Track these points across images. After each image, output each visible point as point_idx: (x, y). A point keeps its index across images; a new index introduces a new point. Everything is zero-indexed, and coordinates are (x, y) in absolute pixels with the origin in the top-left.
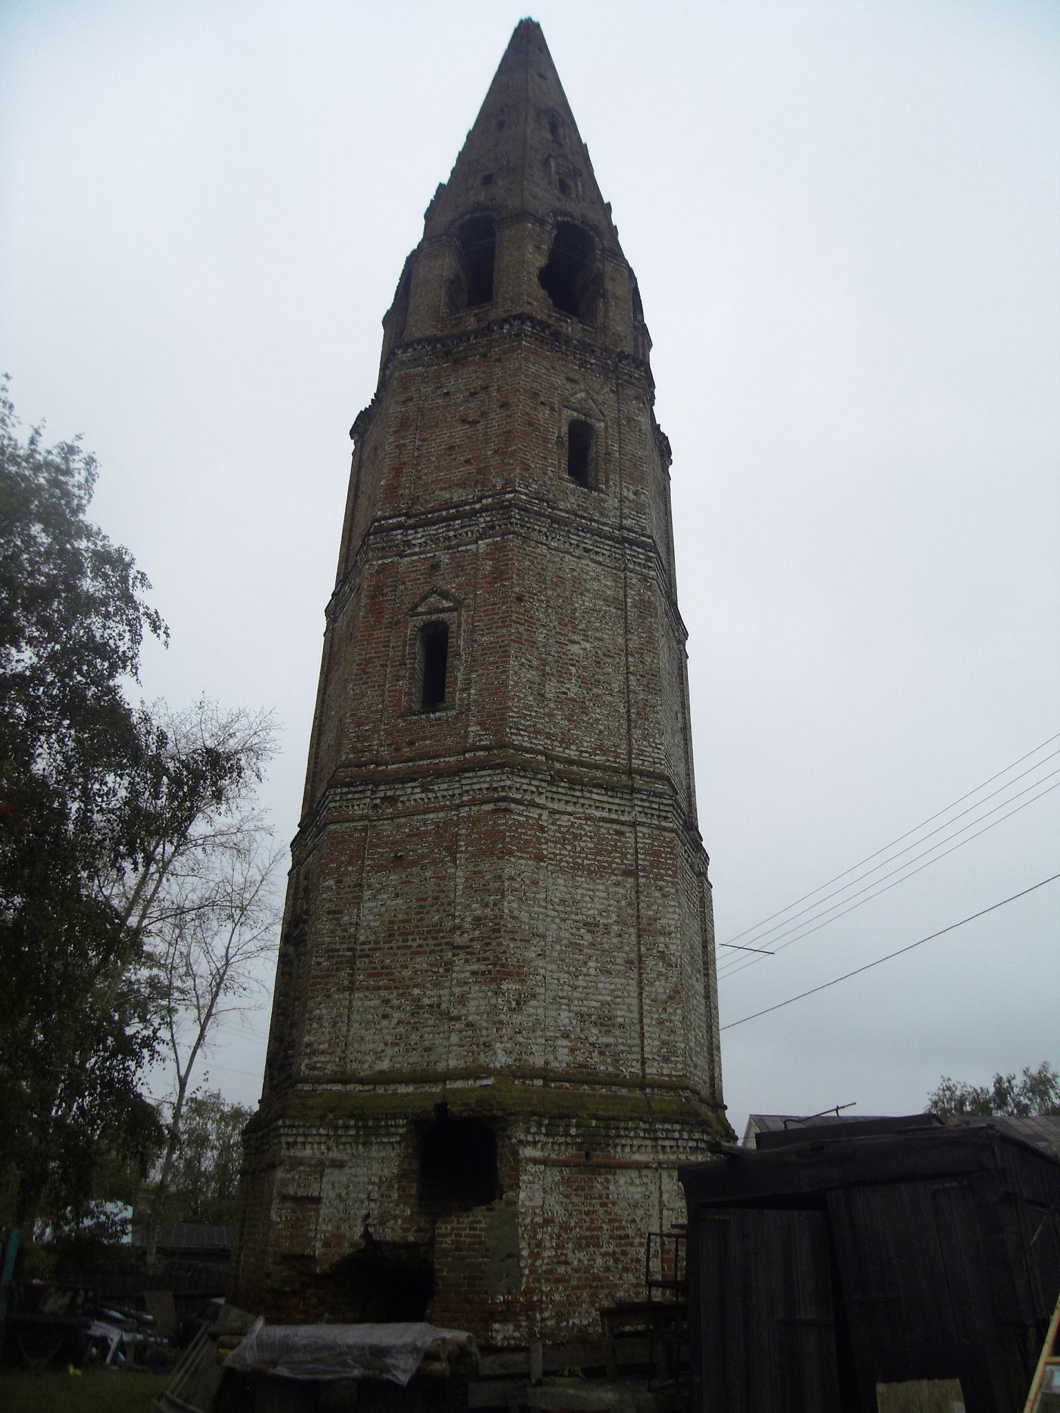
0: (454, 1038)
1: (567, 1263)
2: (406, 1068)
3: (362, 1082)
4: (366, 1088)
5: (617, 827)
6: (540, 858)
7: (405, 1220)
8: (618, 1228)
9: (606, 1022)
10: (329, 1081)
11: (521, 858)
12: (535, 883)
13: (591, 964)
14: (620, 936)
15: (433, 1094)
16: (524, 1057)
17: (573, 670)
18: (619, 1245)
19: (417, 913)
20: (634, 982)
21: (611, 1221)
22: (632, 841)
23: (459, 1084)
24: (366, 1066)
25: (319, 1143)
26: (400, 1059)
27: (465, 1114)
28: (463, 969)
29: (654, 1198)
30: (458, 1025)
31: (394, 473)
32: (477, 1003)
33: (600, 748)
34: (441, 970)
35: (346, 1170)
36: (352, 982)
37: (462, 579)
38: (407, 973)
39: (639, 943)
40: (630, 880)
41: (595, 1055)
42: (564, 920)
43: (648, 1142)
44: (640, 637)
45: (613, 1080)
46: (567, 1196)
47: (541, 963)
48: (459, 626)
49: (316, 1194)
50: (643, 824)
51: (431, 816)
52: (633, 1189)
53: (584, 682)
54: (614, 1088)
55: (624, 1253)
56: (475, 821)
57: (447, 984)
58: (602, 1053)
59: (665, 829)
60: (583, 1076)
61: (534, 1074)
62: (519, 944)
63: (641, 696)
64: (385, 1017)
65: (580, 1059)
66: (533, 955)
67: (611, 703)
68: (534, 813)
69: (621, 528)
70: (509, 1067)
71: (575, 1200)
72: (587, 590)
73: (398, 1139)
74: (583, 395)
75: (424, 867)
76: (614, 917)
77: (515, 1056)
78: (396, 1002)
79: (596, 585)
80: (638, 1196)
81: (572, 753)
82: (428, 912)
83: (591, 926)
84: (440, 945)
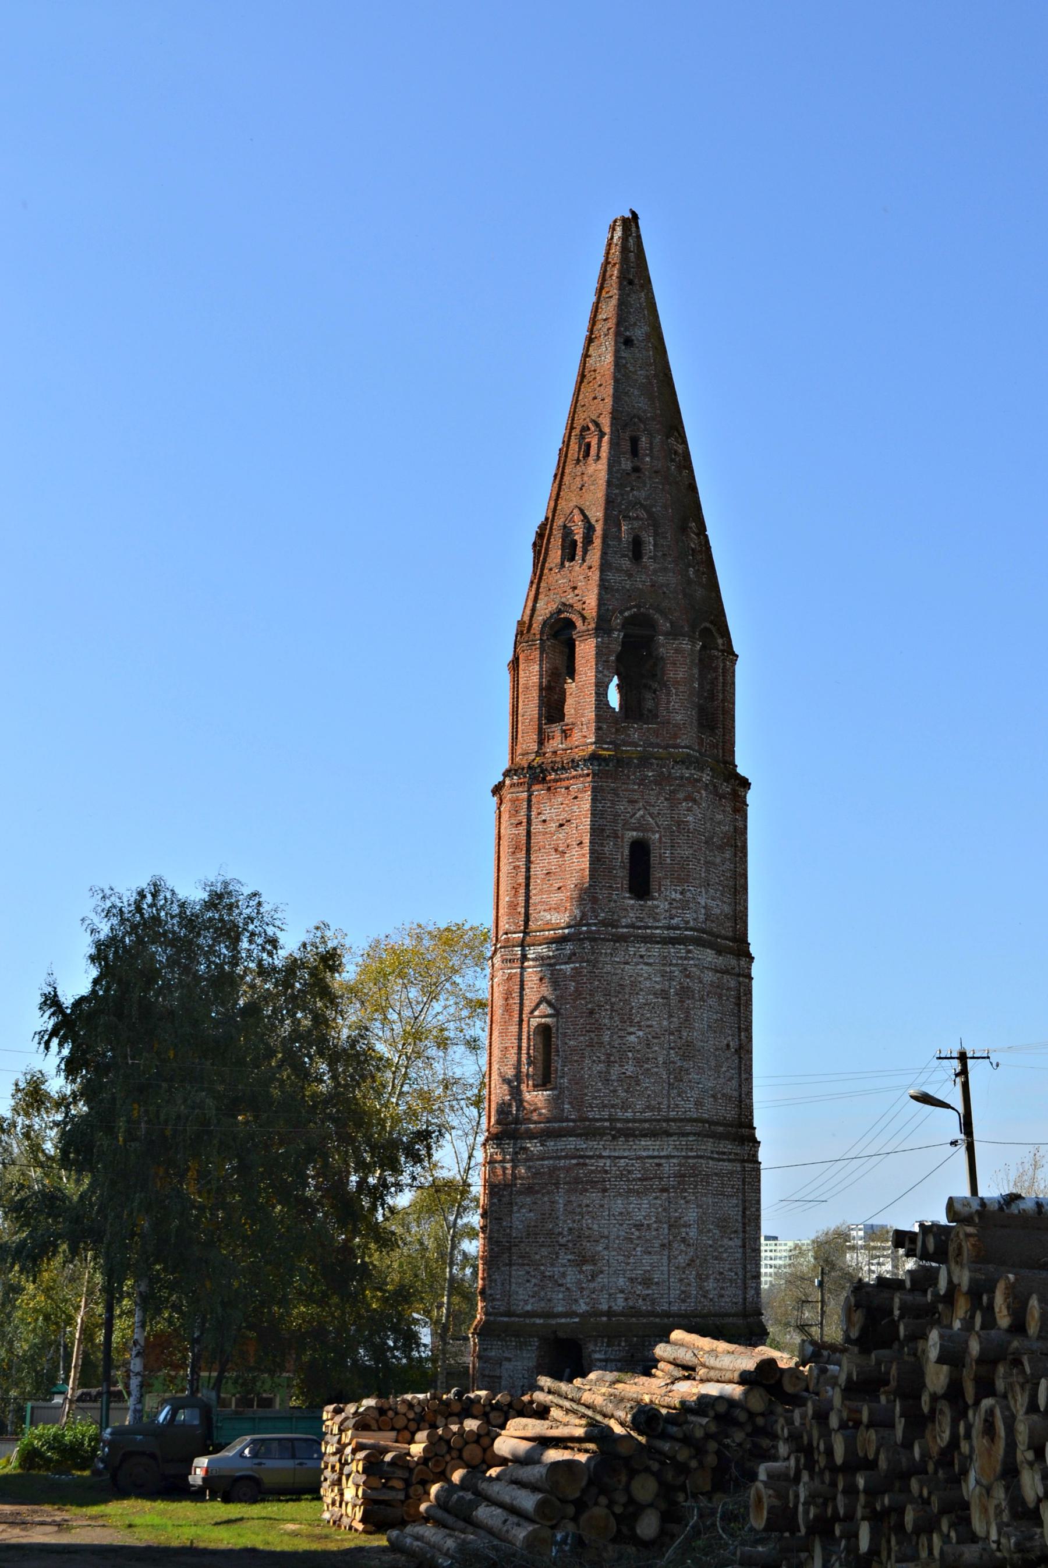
0: (561, 1296)
2: (540, 1310)
3: (518, 1316)
5: (657, 1161)
9: (647, 1282)
10: (502, 1316)
12: (602, 1206)
17: (630, 1054)
28: (564, 1258)
30: (562, 1289)
32: (571, 1277)
33: (649, 1108)
36: (510, 1261)
38: (538, 1257)
40: (665, 1194)
42: (621, 1225)
44: (679, 1018)
47: (606, 1253)
48: (557, 1030)
51: (546, 1162)
53: (639, 1062)
56: (568, 1169)
58: (644, 1300)
59: (689, 1157)
60: (633, 1312)
61: (602, 1314)
63: (679, 1064)
64: (528, 1281)
65: (631, 1304)
67: (657, 1073)
72: (641, 990)
74: (641, 812)
75: (543, 1195)
76: (654, 1219)
79: (648, 984)
81: (629, 1115)
83: (639, 1226)
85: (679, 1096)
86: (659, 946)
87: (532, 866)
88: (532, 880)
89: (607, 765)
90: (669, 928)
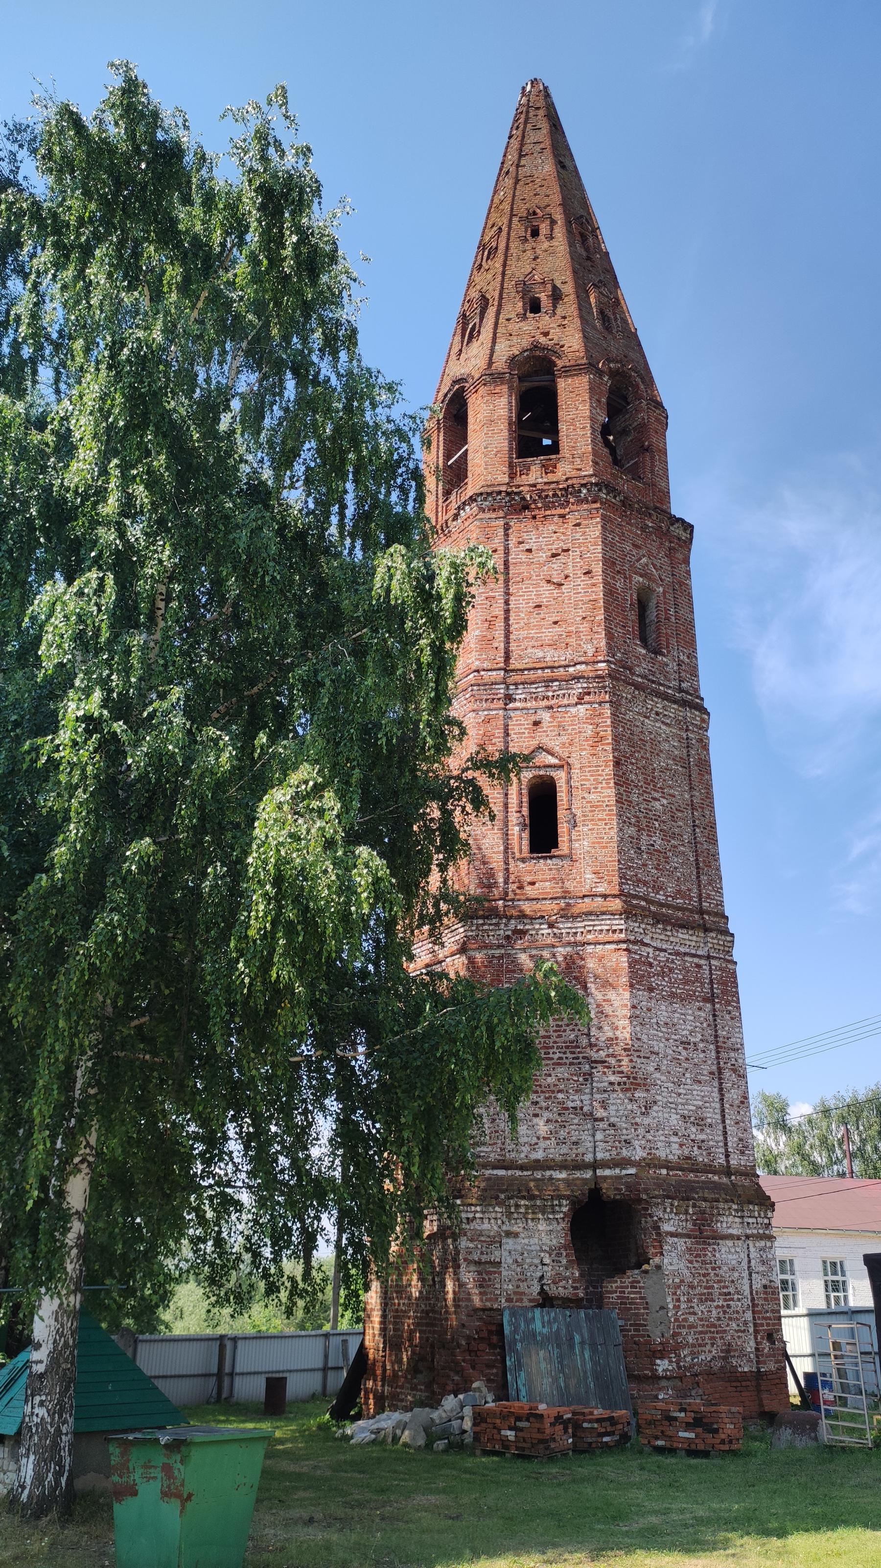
1: (695, 1314)
3: (522, 1168)
4: (525, 1173)
5: (696, 960)
6: (651, 990)
7: (574, 1281)
8: (724, 1287)
9: (700, 1123)
10: (495, 1167)
11: (639, 990)
12: (649, 1010)
13: (688, 1075)
14: (704, 1052)
15: (585, 1180)
16: (653, 1151)
18: (725, 1300)
19: (555, 1031)
20: (716, 1090)
21: (719, 1282)
22: (707, 972)
23: (607, 1172)
24: (523, 1155)
25: (496, 1219)
26: (552, 1150)
27: (618, 1197)
29: (745, 1264)
30: (601, 1125)
31: (486, 625)
34: (581, 1079)
35: (520, 1240)
37: (564, 739)
39: (718, 1058)
40: (708, 1005)
41: (695, 1148)
42: (668, 1040)
43: (737, 1220)
45: (708, 1169)
46: (691, 1262)
49: (498, 1260)
50: (714, 958)
52: (730, 1257)
54: (710, 1176)
55: (729, 1306)
57: (587, 1091)
58: (699, 1148)
60: (689, 1164)
62: (643, 1060)
63: (705, 847)
64: (536, 1115)
65: (686, 1153)
66: (652, 1069)
67: (684, 853)
68: (645, 950)
69: (681, 690)
70: (644, 1159)
71: (696, 1265)
73: (562, 1215)
76: (699, 1036)
77: (647, 1151)
78: (544, 1104)
80: (734, 1262)
81: (661, 897)
82: (565, 1031)
83: (685, 1043)
84: (578, 1058)
85: (710, 884)
86: (675, 706)
87: (512, 598)
88: (512, 614)
89: (615, 497)
90: (681, 690)
